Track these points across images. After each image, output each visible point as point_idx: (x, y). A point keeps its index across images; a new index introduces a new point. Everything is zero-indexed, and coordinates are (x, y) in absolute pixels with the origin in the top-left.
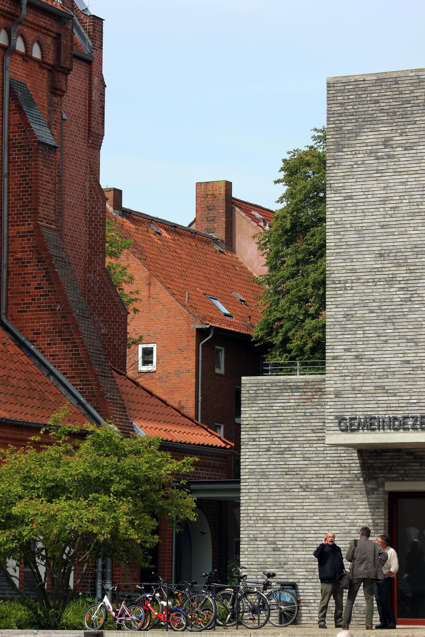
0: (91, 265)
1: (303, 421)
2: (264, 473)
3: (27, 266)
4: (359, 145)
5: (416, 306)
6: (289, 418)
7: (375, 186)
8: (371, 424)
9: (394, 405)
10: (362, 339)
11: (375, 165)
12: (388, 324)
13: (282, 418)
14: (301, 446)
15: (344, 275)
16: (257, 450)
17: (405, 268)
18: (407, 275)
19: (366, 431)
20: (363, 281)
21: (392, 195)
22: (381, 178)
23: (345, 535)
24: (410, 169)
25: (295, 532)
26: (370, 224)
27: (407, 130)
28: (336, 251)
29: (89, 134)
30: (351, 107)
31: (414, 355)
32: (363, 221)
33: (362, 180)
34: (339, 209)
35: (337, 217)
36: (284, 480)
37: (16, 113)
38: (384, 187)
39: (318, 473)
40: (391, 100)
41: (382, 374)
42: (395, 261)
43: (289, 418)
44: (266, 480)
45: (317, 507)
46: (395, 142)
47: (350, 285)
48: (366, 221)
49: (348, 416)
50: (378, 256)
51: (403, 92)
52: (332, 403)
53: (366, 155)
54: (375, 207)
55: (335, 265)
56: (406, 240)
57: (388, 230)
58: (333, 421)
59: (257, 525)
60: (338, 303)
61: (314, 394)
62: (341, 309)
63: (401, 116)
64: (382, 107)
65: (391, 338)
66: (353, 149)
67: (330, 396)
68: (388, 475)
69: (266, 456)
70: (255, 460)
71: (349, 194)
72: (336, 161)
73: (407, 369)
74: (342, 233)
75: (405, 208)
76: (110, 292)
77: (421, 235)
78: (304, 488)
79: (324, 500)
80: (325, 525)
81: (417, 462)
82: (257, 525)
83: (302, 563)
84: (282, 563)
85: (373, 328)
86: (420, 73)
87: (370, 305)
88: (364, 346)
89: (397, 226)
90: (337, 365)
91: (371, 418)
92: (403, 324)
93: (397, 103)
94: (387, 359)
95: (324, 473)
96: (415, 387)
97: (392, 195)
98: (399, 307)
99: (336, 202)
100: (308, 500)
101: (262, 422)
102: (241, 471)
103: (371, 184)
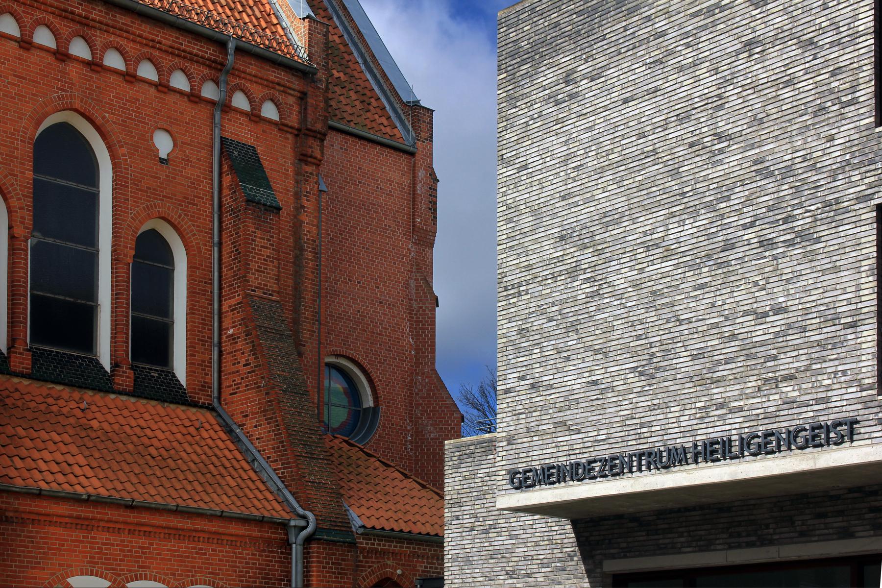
0: (419, 367)
2: (467, 559)
3: (236, 343)
4: (535, 92)
7: (555, 142)
8: (549, 476)
9: (578, 446)
10: (539, 360)
11: (555, 113)
12: (570, 334)
13: (486, 488)
15: (518, 276)
16: (461, 530)
17: (591, 250)
18: (594, 259)
20: (540, 279)
21: (576, 149)
22: (562, 130)
24: (598, 106)
26: (548, 198)
29: (413, 229)
30: (526, 42)
31: (603, 371)
32: (541, 196)
33: (538, 139)
34: (512, 187)
36: (489, 565)
39: (526, 554)
40: (574, 16)
41: (562, 404)
42: (579, 243)
44: (470, 567)
48: (544, 195)
49: (521, 467)
50: (558, 240)
52: (504, 453)
53: (544, 103)
54: (554, 172)
55: (508, 264)
56: (593, 209)
57: (571, 201)
62: (514, 324)
63: (586, 35)
65: (574, 352)
66: (528, 100)
69: (469, 537)
70: (458, 543)
71: (524, 163)
73: (593, 393)
74: (515, 219)
75: (591, 163)
76: (441, 394)
78: (511, 575)
90: (509, 400)
93: (582, 18)
94: (569, 383)
95: (533, 553)
96: (604, 417)
97: (576, 149)
98: (585, 306)
101: (465, 495)
103: (551, 142)
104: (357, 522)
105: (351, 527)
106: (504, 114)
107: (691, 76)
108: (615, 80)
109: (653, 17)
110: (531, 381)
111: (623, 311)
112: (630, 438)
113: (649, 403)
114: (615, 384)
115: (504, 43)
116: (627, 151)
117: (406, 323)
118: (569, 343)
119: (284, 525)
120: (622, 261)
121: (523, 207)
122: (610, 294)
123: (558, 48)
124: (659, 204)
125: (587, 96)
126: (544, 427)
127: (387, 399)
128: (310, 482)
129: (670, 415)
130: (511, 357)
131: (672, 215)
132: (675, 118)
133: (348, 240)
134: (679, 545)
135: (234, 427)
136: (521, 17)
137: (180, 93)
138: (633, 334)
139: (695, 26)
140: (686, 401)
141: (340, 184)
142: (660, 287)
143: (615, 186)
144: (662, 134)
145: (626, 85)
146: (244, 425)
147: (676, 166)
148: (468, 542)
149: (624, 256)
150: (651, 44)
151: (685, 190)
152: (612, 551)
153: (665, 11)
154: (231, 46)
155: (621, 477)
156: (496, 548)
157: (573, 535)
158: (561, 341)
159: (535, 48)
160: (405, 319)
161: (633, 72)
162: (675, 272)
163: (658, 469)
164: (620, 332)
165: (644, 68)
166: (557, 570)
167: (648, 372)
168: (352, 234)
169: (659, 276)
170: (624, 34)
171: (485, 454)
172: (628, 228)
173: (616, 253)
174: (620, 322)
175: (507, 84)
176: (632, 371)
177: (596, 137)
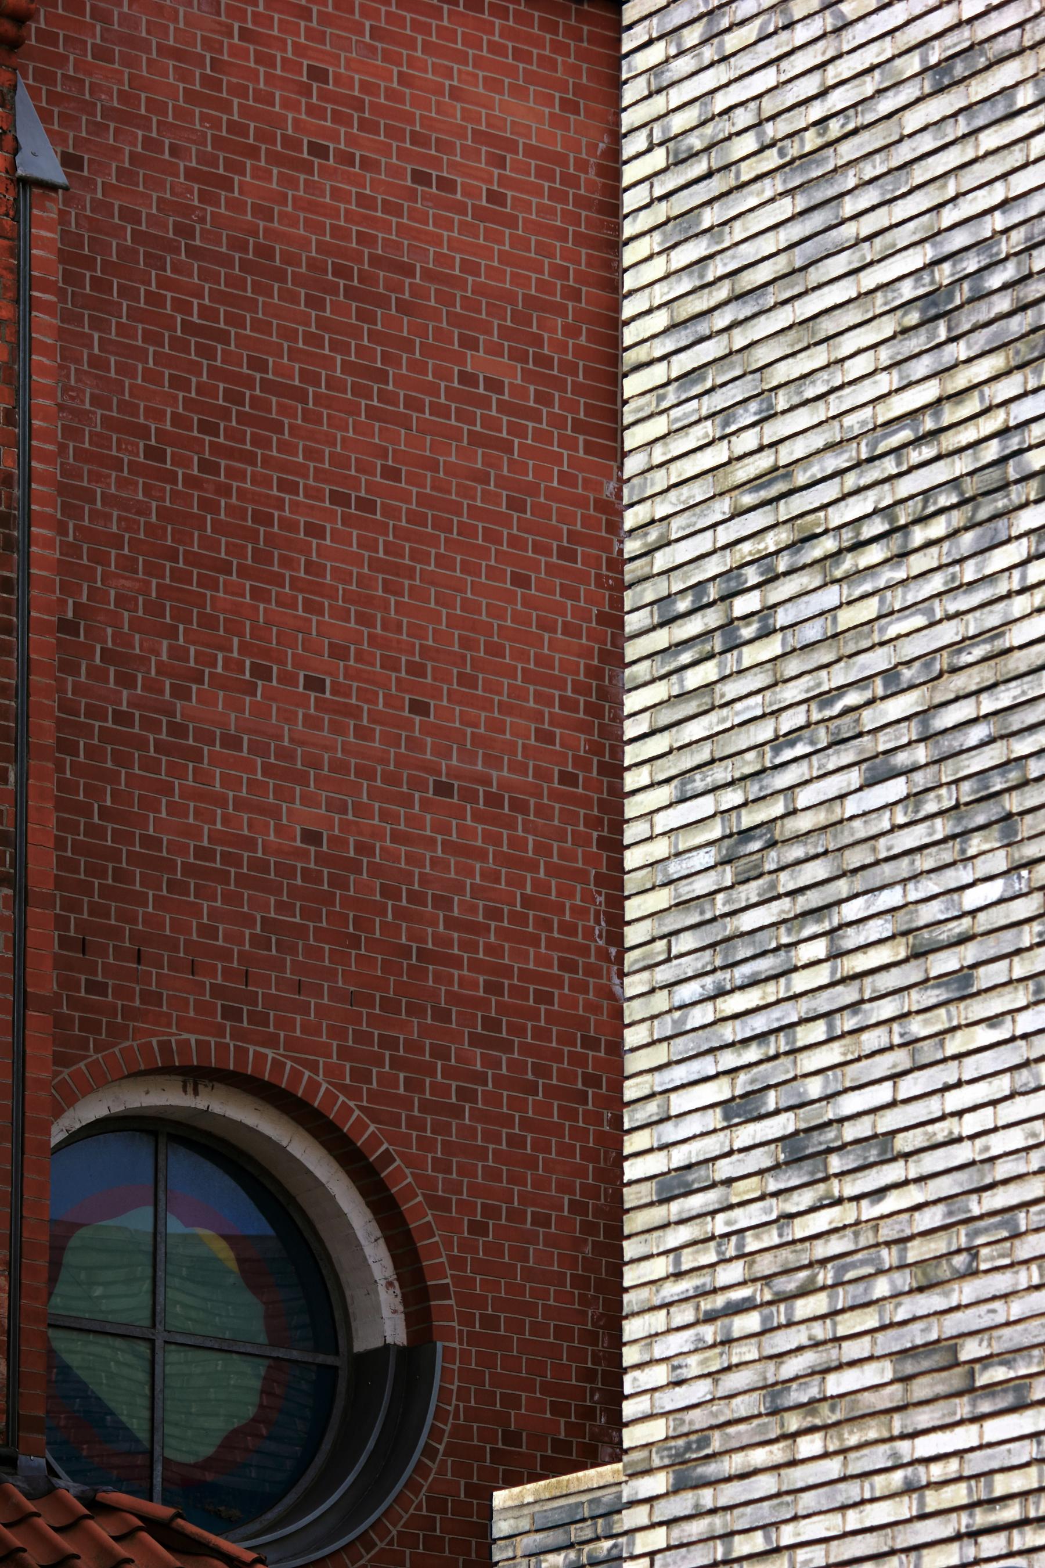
10: (823, 1003)
12: (976, 844)
20: (829, 545)
26: (869, 85)
32: (832, 74)
34: (692, 36)
41: (938, 1245)
50: (913, 318)
57: (979, 89)
62: (705, 806)
74: (709, 218)
94: (971, 1124)
110: (783, 1125)
117: (590, 898)
118: (972, 899)
121: (748, 143)
127: (480, 1302)
130: (688, 992)
133: (249, 458)
141: (202, 158)
158: (930, 886)
160: (580, 875)
168: (277, 426)
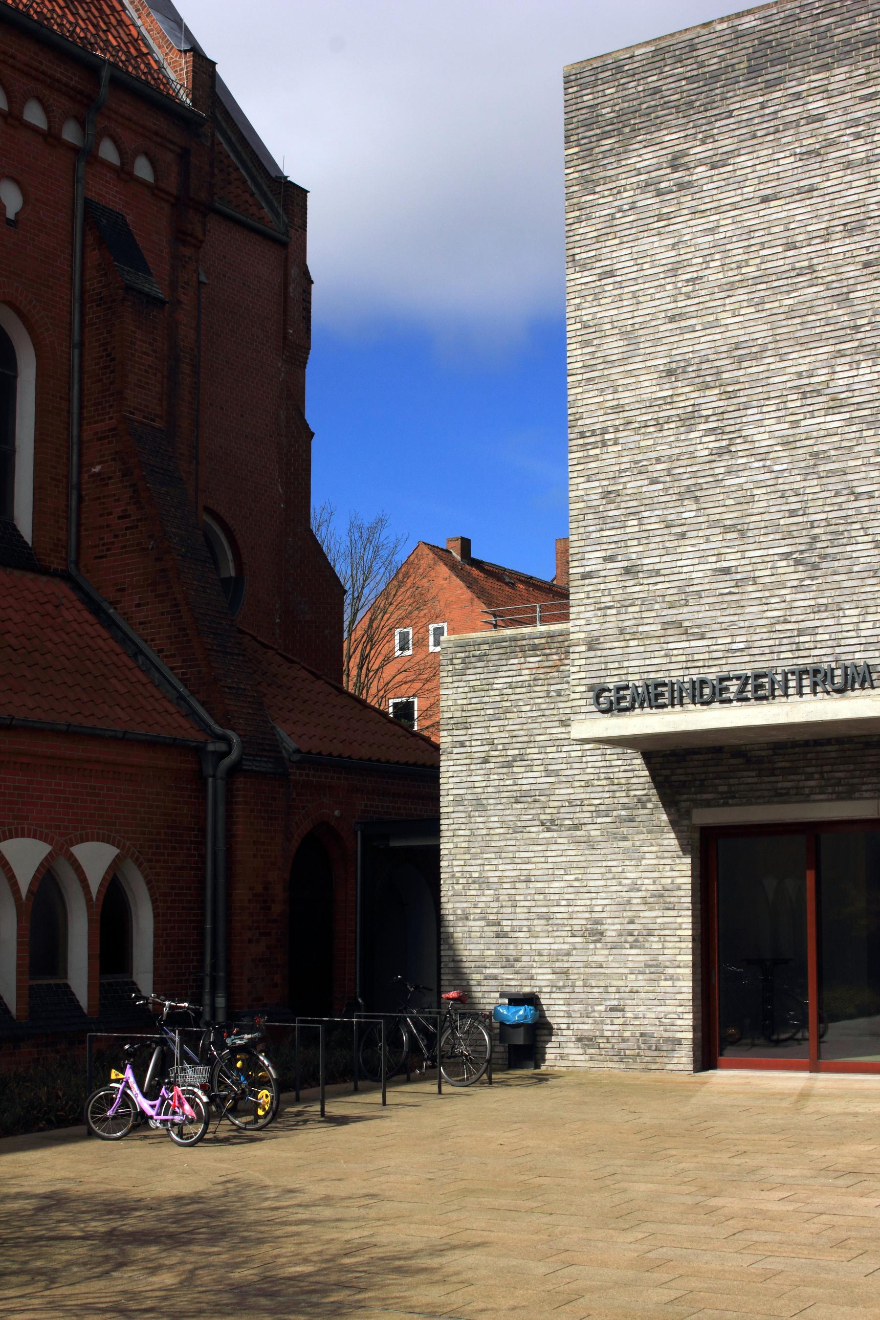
1: (544, 706)
2: (479, 802)
4: (624, 176)
5: (740, 461)
6: (521, 703)
7: (656, 245)
9: (701, 657)
10: (637, 535)
11: (655, 206)
12: (686, 502)
13: (508, 704)
14: (543, 750)
15: (601, 419)
16: (468, 761)
17: (717, 391)
18: (721, 403)
19: (647, 710)
20: (637, 425)
22: (667, 229)
23: (622, 907)
25: (533, 903)
26: (648, 318)
27: (715, 131)
28: (585, 376)
30: (609, 110)
31: (739, 555)
32: (636, 314)
33: (631, 238)
34: (589, 298)
35: (586, 314)
36: (514, 812)
37: (95, 249)
38: (674, 245)
39: (572, 797)
40: (684, 83)
41: (676, 598)
42: (697, 380)
43: (521, 703)
44: (483, 814)
45: (571, 859)
46: (692, 158)
47: (611, 436)
48: (640, 313)
49: (612, 682)
50: (664, 375)
51: (706, 63)
52: (583, 662)
55: (585, 402)
57: (683, 324)
58: (585, 695)
59: (469, 893)
60: (590, 472)
61: (563, 657)
62: (596, 484)
63: (702, 108)
64: (666, 99)
65: (692, 527)
66: (614, 185)
67: (578, 649)
68: (698, 796)
69: (482, 772)
70: (464, 779)
71: (608, 269)
72: (583, 212)
73: (724, 584)
74: (595, 342)
75: (714, 276)
77: (747, 324)
78: (548, 825)
79: (584, 846)
80: (585, 889)
81: (753, 770)
82: (469, 893)
83: (545, 958)
84: (512, 959)
85: (657, 513)
86: (736, 22)
87: (650, 468)
88: (640, 548)
89: (699, 313)
90: (590, 588)
91: (657, 686)
92: (715, 498)
93: (695, 85)
94: (685, 569)
96: (741, 618)
97: (689, 256)
98: (707, 466)
99: (583, 287)
100: (554, 847)
101: (474, 713)
102: (441, 799)
104: (291, 744)
105: (281, 752)
106: (575, 201)
107: (863, 175)
108: (749, 170)
109: (804, 94)
110: (625, 564)
111: (768, 476)
112: (783, 648)
113: (812, 602)
114: (757, 574)
115: (574, 107)
116: (769, 265)
118: (685, 515)
119: (199, 751)
120: (765, 409)
122: (747, 453)
123: (658, 121)
124: (820, 336)
125: (705, 188)
126: (646, 628)
128: (228, 687)
129: (843, 621)
131: (841, 354)
132: (841, 228)
134: (807, 791)
135: (105, 605)
136: (601, 76)
137: (34, 129)
138: (784, 508)
139: (869, 112)
140: (868, 603)
142: (825, 447)
143: (752, 309)
144: (823, 247)
145: (766, 179)
146: (118, 602)
147: (845, 290)
148: (480, 778)
149: (767, 403)
150: (802, 129)
151: (859, 322)
152: (705, 796)
153: (822, 89)
154: (105, 74)
155: (771, 701)
156: (524, 787)
157: (647, 773)
158: (672, 511)
159: (624, 118)
161: (776, 163)
162: (847, 429)
163: (828, 693)
164: (764, 504)
165: (792, 159)
166: (622, 820)
167: (808, 561)
169: (822, 433)
170: (761, 112)
171: (504, 657)
172: (772, 367)
173: (755, 397)
174: (764, 490)
175: (580, 161)
176: (783, 557)
177: (721, 242)
